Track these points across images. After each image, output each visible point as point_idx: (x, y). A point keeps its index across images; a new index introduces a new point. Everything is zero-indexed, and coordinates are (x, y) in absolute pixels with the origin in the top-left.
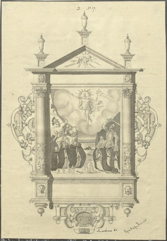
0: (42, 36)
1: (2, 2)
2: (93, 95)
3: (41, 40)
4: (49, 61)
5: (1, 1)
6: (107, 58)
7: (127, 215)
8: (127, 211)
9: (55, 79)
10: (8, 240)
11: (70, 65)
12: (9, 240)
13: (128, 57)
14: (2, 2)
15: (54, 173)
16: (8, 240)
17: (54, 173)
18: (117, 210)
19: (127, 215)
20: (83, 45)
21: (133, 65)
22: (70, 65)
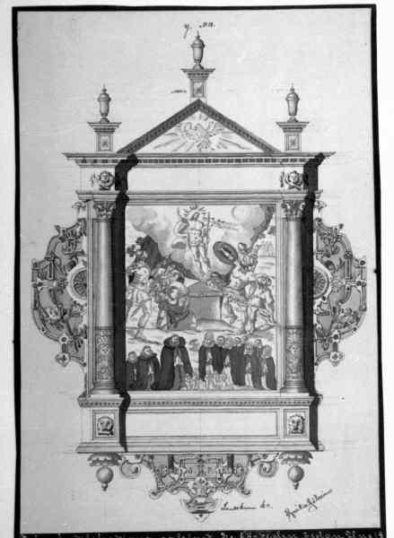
0: (105, 90)
1: (374, 522)
2: (172, 92)
3: (103, 96)
4: (121, 140)
5: (383, 528)
6: (264, 193)
7: (105, 485)
8: (294, 473)
9: (138, 180)
10: (222, 537)
11: (167, 144)
12: (222, 534)
13: (293, 127)
14: (379, 526)
15: (133, 395)
16: (222, 537)
17: (133, 395)
18: (270, 476)
19: (105, 485)
20: (194, 100)
21: (310, 144)
22: (167, 144)
